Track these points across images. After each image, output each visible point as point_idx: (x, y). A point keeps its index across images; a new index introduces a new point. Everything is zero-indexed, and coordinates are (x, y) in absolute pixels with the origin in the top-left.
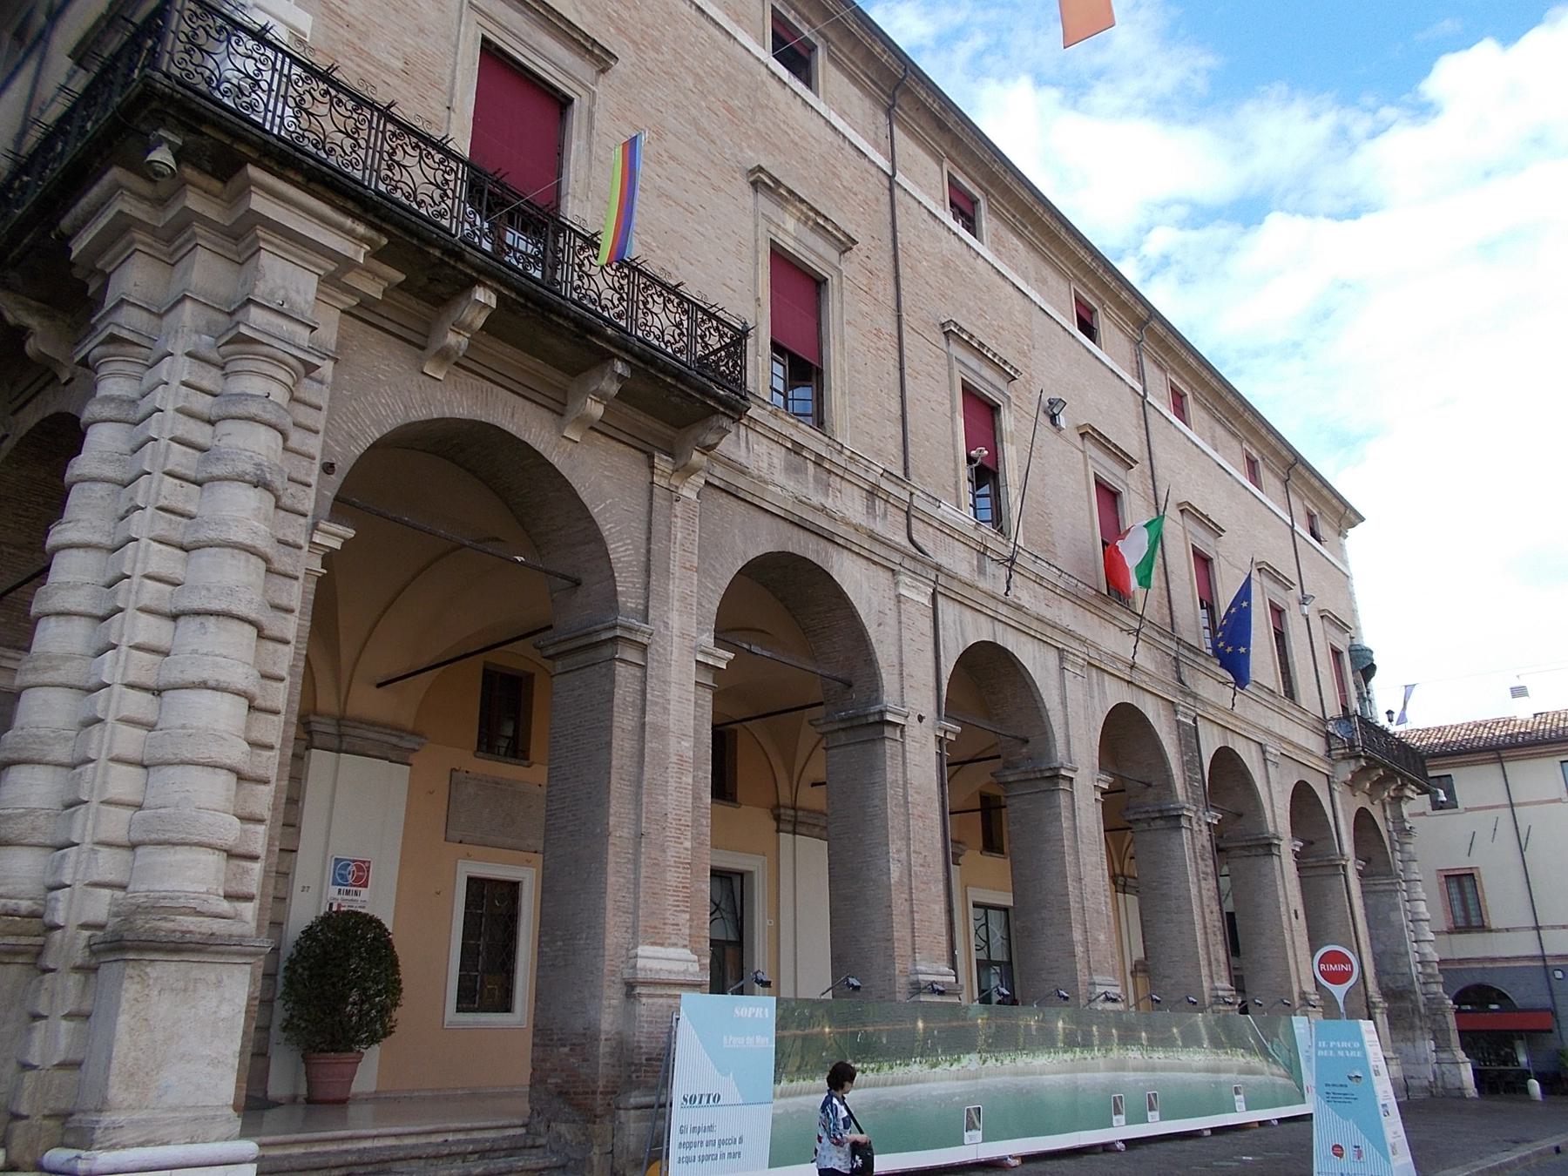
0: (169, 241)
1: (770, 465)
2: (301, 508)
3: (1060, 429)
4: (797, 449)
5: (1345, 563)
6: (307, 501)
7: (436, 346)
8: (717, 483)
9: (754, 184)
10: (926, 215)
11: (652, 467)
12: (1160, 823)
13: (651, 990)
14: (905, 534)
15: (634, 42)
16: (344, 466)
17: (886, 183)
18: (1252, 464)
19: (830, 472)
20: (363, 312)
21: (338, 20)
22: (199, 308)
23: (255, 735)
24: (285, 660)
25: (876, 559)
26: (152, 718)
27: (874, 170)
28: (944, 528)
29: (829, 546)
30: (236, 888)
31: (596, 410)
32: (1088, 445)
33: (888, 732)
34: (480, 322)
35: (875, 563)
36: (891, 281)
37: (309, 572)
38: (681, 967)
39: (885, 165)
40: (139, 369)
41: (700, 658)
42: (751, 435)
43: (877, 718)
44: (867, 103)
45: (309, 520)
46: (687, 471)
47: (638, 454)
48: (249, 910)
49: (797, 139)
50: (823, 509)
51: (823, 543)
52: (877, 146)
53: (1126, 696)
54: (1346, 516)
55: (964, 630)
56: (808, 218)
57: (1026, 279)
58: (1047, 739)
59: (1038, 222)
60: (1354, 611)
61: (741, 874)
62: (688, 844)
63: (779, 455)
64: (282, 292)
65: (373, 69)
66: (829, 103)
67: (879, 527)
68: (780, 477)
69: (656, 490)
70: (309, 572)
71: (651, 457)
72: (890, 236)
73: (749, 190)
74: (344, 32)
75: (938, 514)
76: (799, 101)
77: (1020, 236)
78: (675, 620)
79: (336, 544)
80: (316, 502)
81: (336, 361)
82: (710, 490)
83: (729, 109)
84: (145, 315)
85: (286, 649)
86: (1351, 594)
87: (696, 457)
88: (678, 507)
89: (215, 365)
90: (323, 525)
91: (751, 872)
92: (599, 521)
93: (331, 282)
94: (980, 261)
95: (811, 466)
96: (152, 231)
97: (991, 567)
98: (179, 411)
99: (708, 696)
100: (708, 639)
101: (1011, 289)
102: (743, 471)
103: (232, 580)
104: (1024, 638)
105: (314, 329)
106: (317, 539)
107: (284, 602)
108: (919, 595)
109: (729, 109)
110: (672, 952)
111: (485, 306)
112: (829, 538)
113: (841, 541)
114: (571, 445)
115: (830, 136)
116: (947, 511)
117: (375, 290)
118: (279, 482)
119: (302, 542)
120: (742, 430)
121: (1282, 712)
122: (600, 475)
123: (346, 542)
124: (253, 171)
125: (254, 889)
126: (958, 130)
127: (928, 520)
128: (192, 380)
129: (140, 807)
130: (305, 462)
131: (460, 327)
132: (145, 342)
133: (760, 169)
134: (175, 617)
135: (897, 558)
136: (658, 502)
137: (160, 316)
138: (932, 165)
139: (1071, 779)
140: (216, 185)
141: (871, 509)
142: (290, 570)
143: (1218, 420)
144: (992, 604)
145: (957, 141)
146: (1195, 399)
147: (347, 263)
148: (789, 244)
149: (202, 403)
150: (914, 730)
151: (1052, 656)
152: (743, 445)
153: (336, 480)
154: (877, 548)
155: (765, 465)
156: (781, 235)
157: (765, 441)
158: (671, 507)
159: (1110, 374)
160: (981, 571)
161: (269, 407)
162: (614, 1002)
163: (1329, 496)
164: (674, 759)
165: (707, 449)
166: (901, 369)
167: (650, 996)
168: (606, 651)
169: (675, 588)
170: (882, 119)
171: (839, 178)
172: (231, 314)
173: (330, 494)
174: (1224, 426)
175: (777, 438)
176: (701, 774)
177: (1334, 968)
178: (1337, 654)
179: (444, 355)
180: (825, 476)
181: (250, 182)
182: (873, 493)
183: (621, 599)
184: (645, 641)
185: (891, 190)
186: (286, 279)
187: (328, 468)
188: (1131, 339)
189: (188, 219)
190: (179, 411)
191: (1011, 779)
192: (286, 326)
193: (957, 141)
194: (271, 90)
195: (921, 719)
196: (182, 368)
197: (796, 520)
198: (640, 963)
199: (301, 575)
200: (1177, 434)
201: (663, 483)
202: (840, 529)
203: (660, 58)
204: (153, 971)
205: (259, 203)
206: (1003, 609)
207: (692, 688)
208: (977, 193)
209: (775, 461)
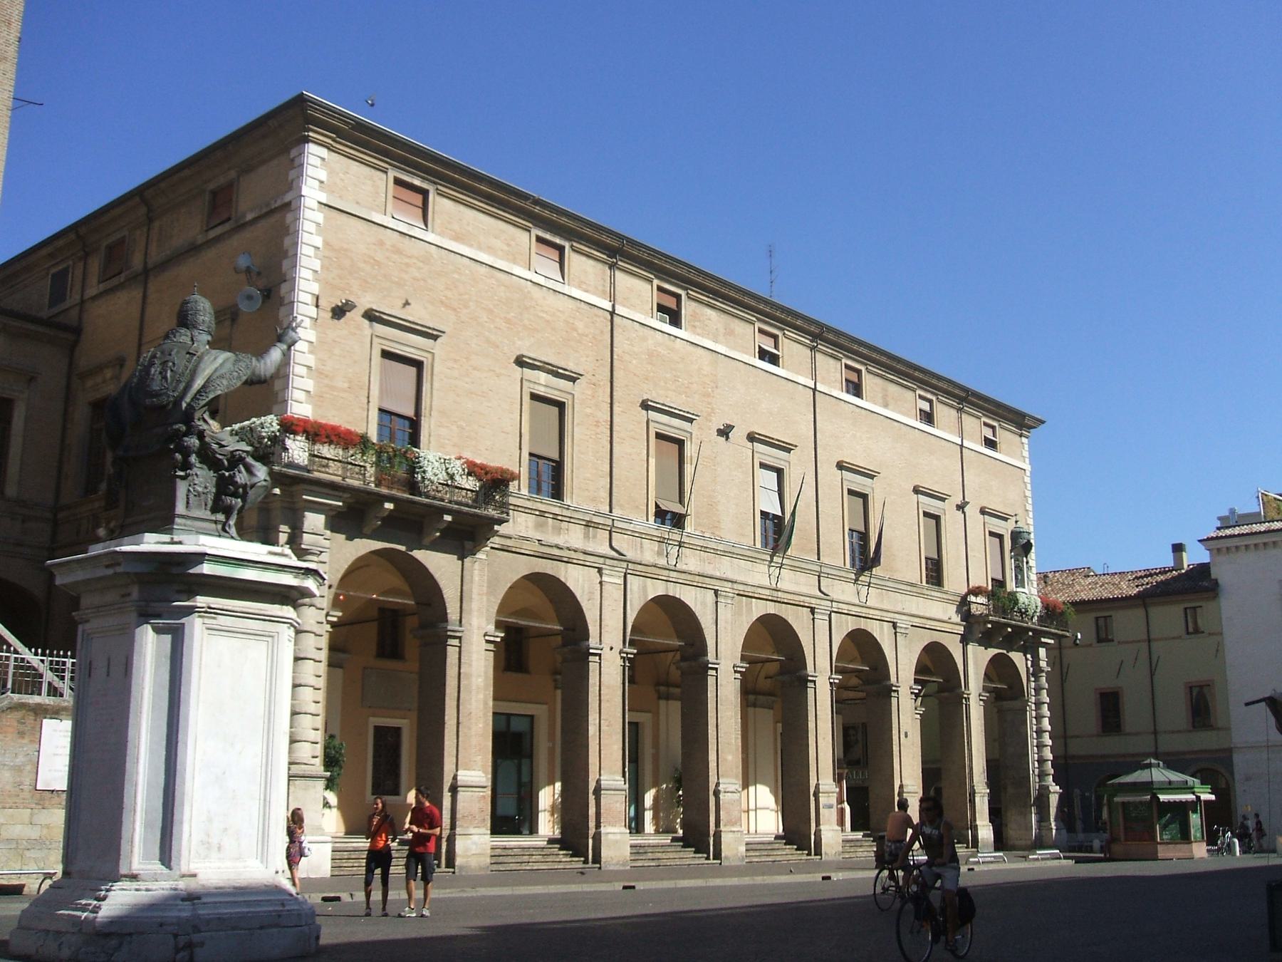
4: (542, 514)
49: (548, 318)
52: (601, 294)
53: (771, 609)
55: (644, 590)
83: (508, 321)
109: (508, 321)
110: (473, 773)
115: (571, 303)
135: (601, 560)
206: (673, 574)
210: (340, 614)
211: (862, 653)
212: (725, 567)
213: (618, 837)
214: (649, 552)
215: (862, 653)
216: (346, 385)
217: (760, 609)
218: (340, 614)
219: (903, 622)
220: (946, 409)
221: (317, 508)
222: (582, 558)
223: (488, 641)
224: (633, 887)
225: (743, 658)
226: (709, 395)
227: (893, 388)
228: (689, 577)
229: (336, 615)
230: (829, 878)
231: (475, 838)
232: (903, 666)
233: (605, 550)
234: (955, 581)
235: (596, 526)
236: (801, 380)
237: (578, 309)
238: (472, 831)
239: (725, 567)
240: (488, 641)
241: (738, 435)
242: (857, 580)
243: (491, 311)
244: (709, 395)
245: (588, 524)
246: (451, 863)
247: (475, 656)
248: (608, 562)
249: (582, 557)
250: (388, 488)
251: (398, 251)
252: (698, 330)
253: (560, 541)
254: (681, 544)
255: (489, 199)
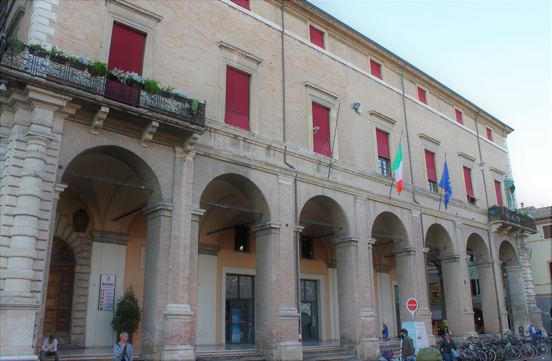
0: (12, 106)
1: (224, 144)
2: (51, 180)
3: (359, 113)
4: (236, 137)
5: (505, 147)
6: (53, 178)
7: (93, 126)
8: (201, 153)
9: (220, 46)
10: (298, 42)
11: (175, 151)
12: (405, 254)
13: (173, 317)
14: (283, 161)
15: (172, 9)
16: (65, 166)
17: (280, 34)
18: (459, 114)
19: (250, 143)
20: (70, 118)
21: (63, 28)
22: (19, 126)
23: (39, 247)
24: (46, 225)
25: (269, 171)
26: (8, 244)
27: (275, 31)
28: (301, 157)
29: (248, 169)
30: (34, 289)
31: (150, 137)
32: (373, 117)
33: (273, 231)
34: (105, 116)
35: (269, 173)
36: (281, 70)
37: (54, 199)
38: (184, 310)
39: (279, 28)
40: (5, 144)
41: (193, 212)
42: (216, 134)
43: (269, 226)
44: (273, 7)
45: (54, 184)
46: (188, 152)
47: (170, 148)
48: (39, 295)
49: (240, 27)
50: (245, 157)
51: (246, 168)
52: (276, 22)
53: (387, 209)
54: (506, 130)
55: (308, 192)
56: (243, 55)
57: (346, 59)
58: (348, 227)
59: (351, 37)
60: (508, 166)
61: (316, 281)
62: (188, 272)
63: (228, 140)
64: (42, 119)
65: (75, 41)
66: (255, 12)
67: (271, 160)
68: (228, 148)
69: (177, 159)
70: (54, 199)
71: (175, 148)
72: (281, 53)
73: (219, 49)
74: (66, 32)
75: (298, 152)
76: (242, 13)
77: (344, 43)
78: (184, 201)
79: (63, 190)
80: (57, 177)
81: (62, 135)
82: (198, 156)
83: (211, 22)
84: (7, 129)
85: (48, 222)
86: (508, 159)
87: (189, 147)
88: (185, 164)
89: (24, 142)
90: (58, 185)
91: (319, 280)
92: (155, 172)
93: (59, 110)
94: (324, 56)
95: (242, 142)
96: (7, 104)
97: (323, 169)
98: (14, 157)
99: (197, 224)
100: (197, 206)
101: (339, 64)
102: (211, 148)
103: (26, 205)
104: (338, 192)
105: (52, 128)
106: (57, 189)
107: (47, 208)
108: (289, 182)
109: (211, 22)
110: (181, 305)
111: (105, 112)
112: (248, 166)
113: (254, 167)
114: (144, 148)
115: (255, 22)
116: (302, 151)
117: (73, 112)
118: (41, 175)
119: (51, 191)
120: (213, 133)
121: (471, 210)
122: (156, 158)
123: (65, 189)
124: (28, 86)
125: (40, 289)
126: (312, 11)
127: (293, 155)
128: (18, 148)
129: (6, 268)
130: (52, 167)
131: (99, 119)
132: (6, 137)
133: (222, 42)
134: (14, 216)
135: (278, 170)
136: (177, 163)
137: (11, 128)
138: (304, 24)
139: (357, 241)
140: (21, 91)
141: (268, 154)
142: (48, 199)
143: (442, 99)
144: (322, 182)
145: (312, 14)
146: (430, 92)
147: (62, 107)
148: (235, 65)
149: (20, 154)
150: (284, 229)
151: (351, 198)
152: (213, 138)
153: (63, 170)
154: (269, 168)
155: (222, 144)
156: (231, 62)
157: (222, 136)
158: (182, 164)
159: (387, 89)
160: (318, 170)
161: (38, 154)
162: (161, 320)
163: (496, 123)
164: (182, 245)
165: (192, 144)
166: (284, 102)
167: (171, 318)
168: (159, 213)
169: (183, 191)
170: (280, 11)
171: (258, 37)
172: (29, 126)
173: (61, 175)
174: (445, 101)
175: (227, 134)
176: (194, 250)
177: (412, 305)
178: (497, 183)
179: (96, 128)
180: (248, 144)
181: (29, 89)
182: (269, 148)
183: (163, 196)
184: (171, 209)
185: (282, 37)
186: (44, 115)
187: (60, 167)
188: (398, 74)
189: (14, 101)
190: (14, 157)
191: (337, 242)
192: (43, 128)
193: (312, 14)
194: (33, 61)
195: (287, 225)
196: (15, 144)
197: (234, 162)
198: (169, 309)
199: (52, 200)
200: (420, 107)
201: (180, 156)
202: (254, 163)
203: (183, 11)
204: (7, 312)
205: (32, 95)
206: (326, 183)
207: (190, 222)
208: (323, 30)
209: (227, 142)
210: (205, 211)
211: (436, 235)
212: (359, 183)
213: (294, 348)
214: (308, 168)
215: (436, 235)
216: (84, 37)
217: (381, 209)
218: (205, 211)
219: (459, 222)
220: (469, 118)
222: (269, 169)
225: (373, 236)
226: (344, 87)
227: (442, 103)
229: (62, 188)
231: (180, 352)
232: (459, 243)
233: (281, 164)
234: (482, 204)
236: (396, 89)
237: (260, 26)
238: (179, 347)
239: (359, 183)
243: (198, 14)
244: (344, 87)
245: (269, 148)
248: (283, 171)
254: (330, 166)
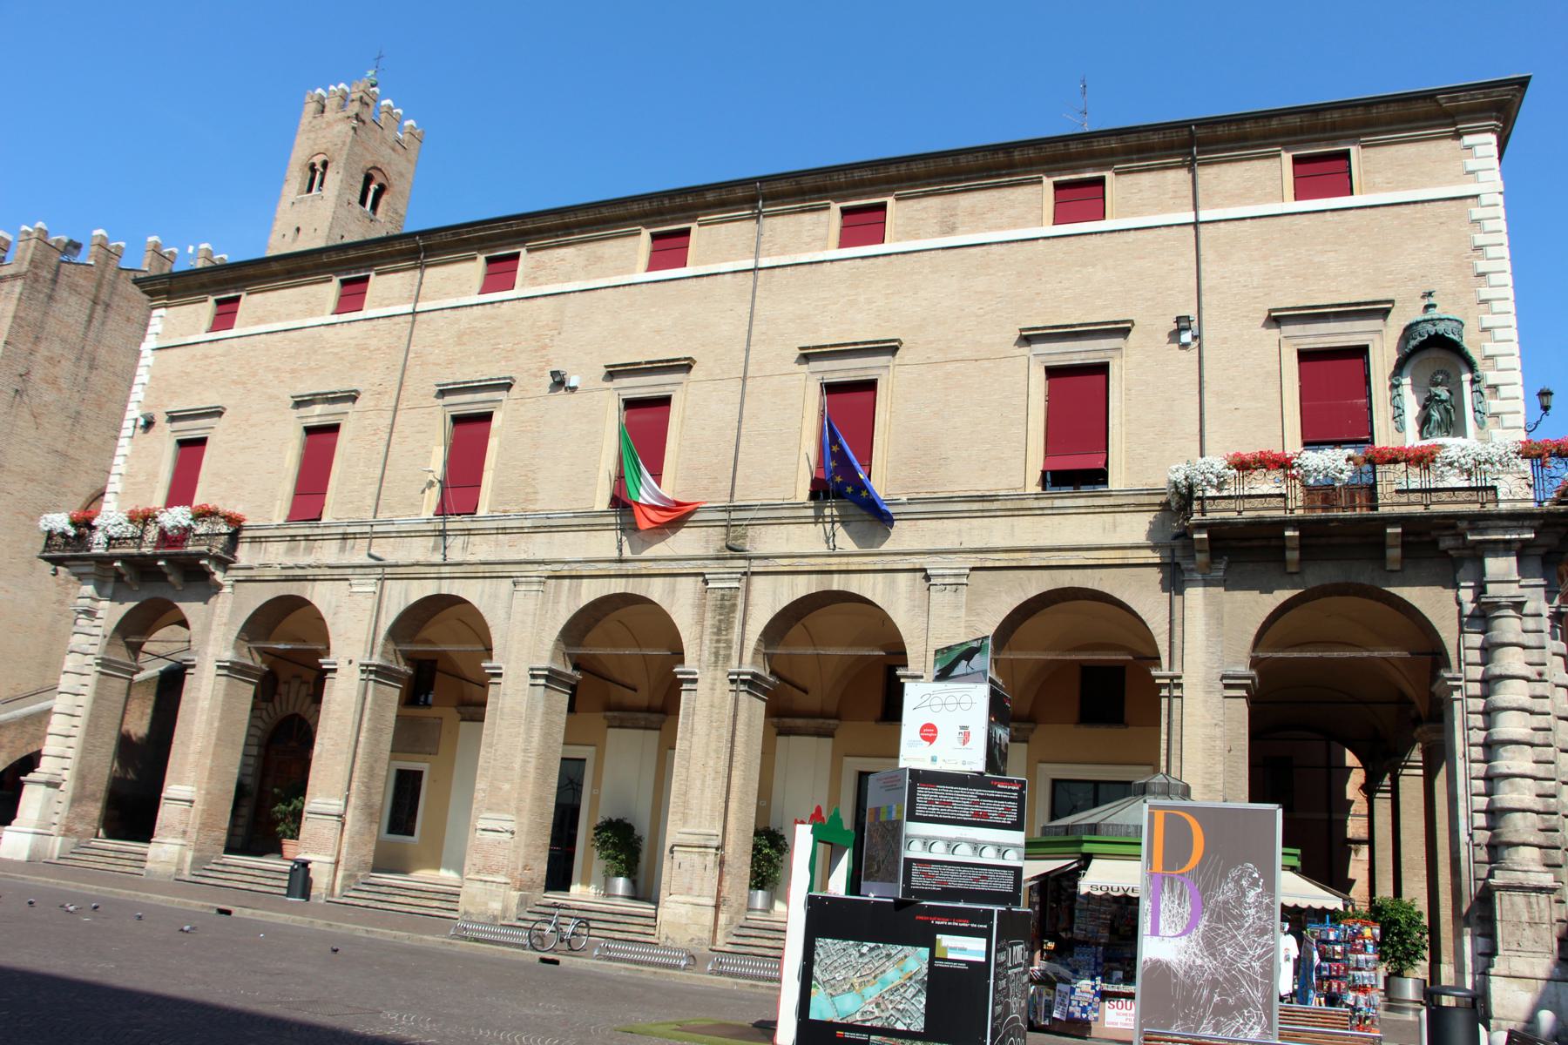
4: (293, 538)
221: (1503, 548)
223: (733, 681)
224: (556, 962)
228: (469, 568)
230: (228, 913)
235: (354, 536)
240: (733, 681)
241: (161, 419)
242: (234, 539)
245: (344, 537)
246: (1104, 996)
247: (206, 674)
249: (328, 571)
250: (1324, 509)
251: (206, 357)
252: (541, 280)
253: (304, 561)
255: (583, 226)
